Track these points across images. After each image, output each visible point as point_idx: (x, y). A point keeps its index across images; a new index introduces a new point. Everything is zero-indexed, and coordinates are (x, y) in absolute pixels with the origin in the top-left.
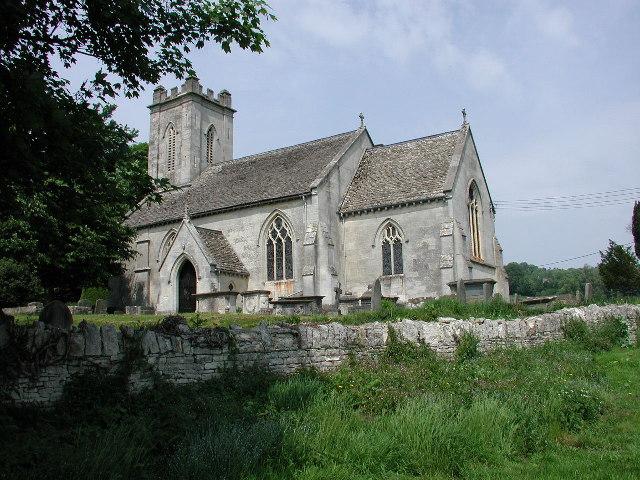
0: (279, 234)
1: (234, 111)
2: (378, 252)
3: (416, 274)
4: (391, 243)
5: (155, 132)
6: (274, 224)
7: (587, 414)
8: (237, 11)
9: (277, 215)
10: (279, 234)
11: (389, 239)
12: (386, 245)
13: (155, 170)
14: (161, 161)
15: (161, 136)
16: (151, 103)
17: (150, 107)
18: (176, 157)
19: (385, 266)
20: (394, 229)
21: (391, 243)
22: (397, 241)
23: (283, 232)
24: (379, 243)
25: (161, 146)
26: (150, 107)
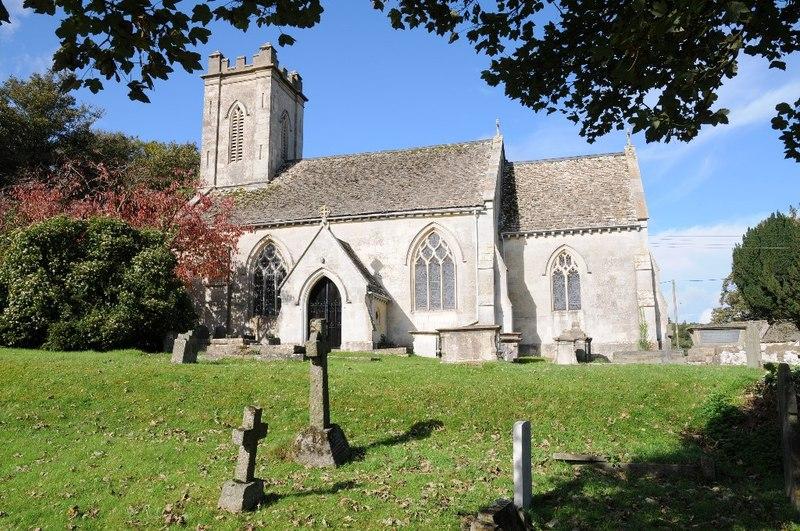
1: (306, 100)
3: (601, 311)
9: (433, 229)
11: (561, 269)
21: (565, 273)
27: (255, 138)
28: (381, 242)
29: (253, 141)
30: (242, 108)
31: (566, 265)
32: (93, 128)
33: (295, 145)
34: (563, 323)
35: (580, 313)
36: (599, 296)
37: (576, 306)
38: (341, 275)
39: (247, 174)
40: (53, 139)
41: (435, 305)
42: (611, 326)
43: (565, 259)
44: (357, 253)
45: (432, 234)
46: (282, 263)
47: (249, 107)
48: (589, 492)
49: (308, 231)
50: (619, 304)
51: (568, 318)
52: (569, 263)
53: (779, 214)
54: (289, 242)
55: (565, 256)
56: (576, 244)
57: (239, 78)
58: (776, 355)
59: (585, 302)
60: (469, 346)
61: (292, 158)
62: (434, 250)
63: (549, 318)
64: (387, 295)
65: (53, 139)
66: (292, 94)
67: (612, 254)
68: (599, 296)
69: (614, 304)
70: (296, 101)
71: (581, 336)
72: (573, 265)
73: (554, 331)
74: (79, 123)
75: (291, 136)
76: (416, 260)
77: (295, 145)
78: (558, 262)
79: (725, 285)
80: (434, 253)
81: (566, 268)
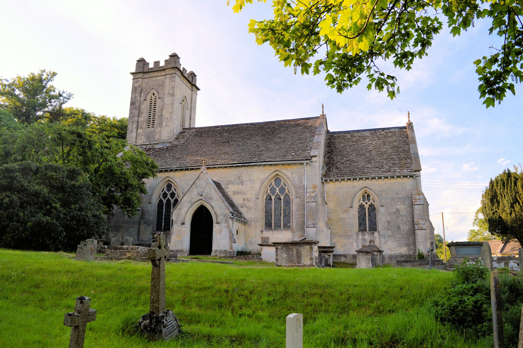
0: (169, 196)
1: (198, 89)
2: (354, 213)
3: (389, 233)
4: (367, 206)
5: (138, 95)
6: (273, 183)
7: (37, 286)
8: (44, 73)
9: (277, 175)
10: (169, 196)
11: (364, 203)
12: (362, 207)
13: (135, 126)
14: (141, 119)
15: (142, 99)
16: (134, 70)
17: (132, 74)
18: (156, 117)
19: (360, 225)
20: (368, 196)
21: (367, 206)
22: (371, 206)
23: (282, 190)
24: (356, 205)
25: (143, 107)
26: (132, 74)
27: (163, 113)
28: (242, 183)
29: (162, 115)
30: (156, 94)
31: (366, 201)
32: (64, 106)
33: (190, 119)
34: (364, 240)
35: (376, 234)
36: (388, 222)
37: (373, 228)
38: (213, 204)
39: (157, 137)
40: (40, 113)
41: (278, 227)
42: (397, 243)
43: (367, 197)
44: (226, 190)
45: (277, 180)
46: (176, 196)
47: (160, 93)
48: (512, 65)
49: (191, 175)
50: (402, 228)
51: (367, 237)
52: (369, 200)
53: (508, 169)
54: (181, 180)
55: (366, 195)
56: (375, 186)
57: (155, 74)
58: (503, 263)
59: (380, 225)
60: (295, 254)
61: (188, 127)
62: (277, 189)
63: (355, 236)
64: (245, 218)
65: (40, 113)
66: (189, 85)
67: (398, 194)
68: (388, 222)
69: (399, 228)
70: (192, 90)
71: (376, 249)
72: (371, 201)
73: (358, 246)
74: (55, 103)
75: (188, 112)
76: (265, 196)
77: (190, 119)
78: (362, 199)
79: (477, 213)
80: (277, 191)
81: (366, 203)
